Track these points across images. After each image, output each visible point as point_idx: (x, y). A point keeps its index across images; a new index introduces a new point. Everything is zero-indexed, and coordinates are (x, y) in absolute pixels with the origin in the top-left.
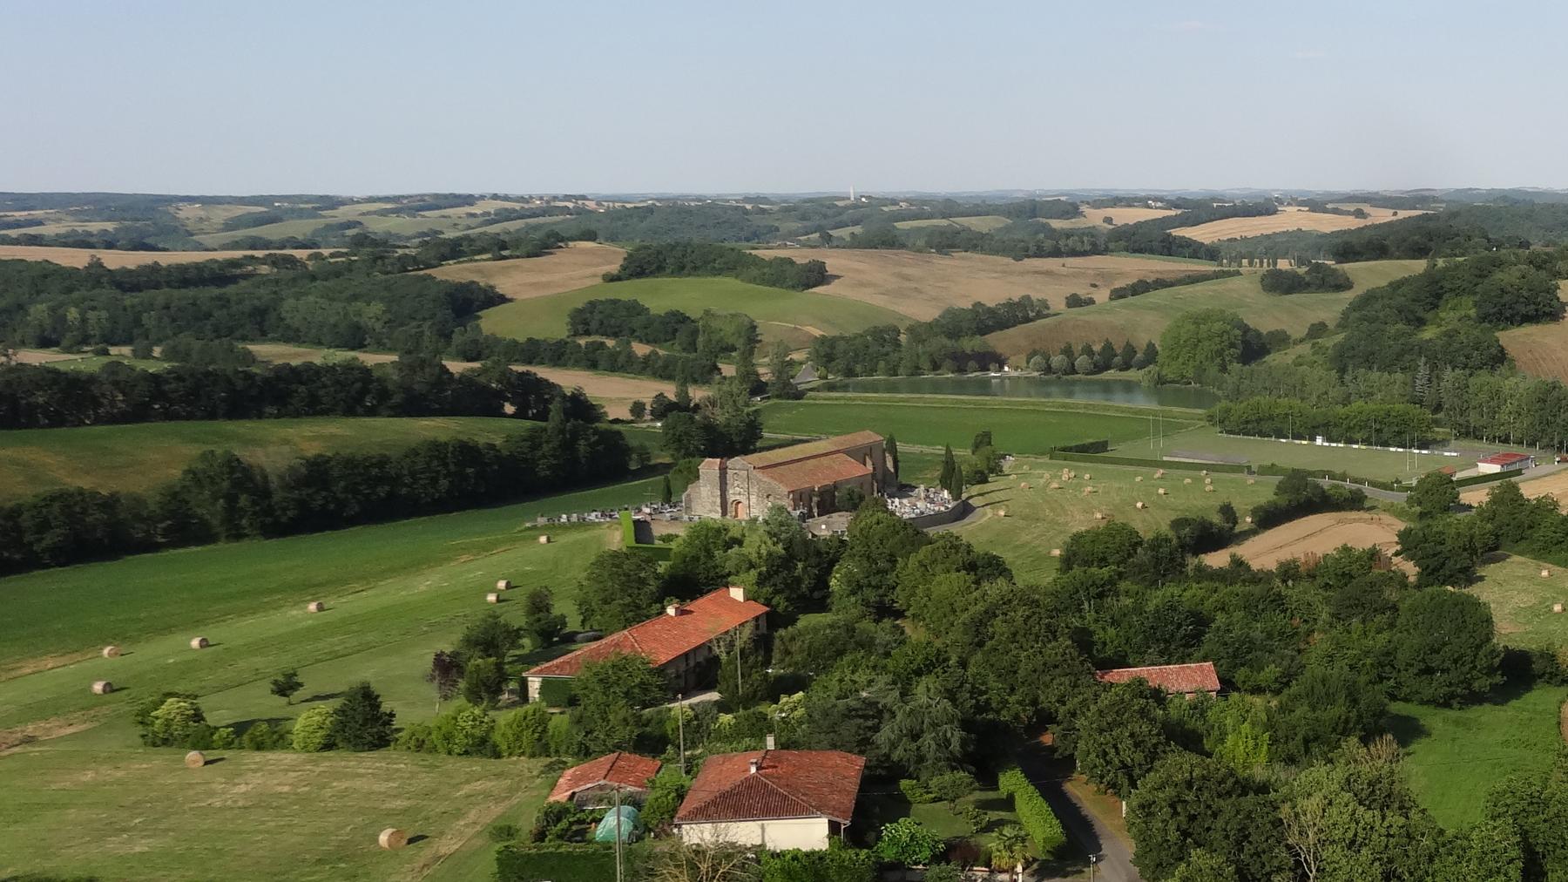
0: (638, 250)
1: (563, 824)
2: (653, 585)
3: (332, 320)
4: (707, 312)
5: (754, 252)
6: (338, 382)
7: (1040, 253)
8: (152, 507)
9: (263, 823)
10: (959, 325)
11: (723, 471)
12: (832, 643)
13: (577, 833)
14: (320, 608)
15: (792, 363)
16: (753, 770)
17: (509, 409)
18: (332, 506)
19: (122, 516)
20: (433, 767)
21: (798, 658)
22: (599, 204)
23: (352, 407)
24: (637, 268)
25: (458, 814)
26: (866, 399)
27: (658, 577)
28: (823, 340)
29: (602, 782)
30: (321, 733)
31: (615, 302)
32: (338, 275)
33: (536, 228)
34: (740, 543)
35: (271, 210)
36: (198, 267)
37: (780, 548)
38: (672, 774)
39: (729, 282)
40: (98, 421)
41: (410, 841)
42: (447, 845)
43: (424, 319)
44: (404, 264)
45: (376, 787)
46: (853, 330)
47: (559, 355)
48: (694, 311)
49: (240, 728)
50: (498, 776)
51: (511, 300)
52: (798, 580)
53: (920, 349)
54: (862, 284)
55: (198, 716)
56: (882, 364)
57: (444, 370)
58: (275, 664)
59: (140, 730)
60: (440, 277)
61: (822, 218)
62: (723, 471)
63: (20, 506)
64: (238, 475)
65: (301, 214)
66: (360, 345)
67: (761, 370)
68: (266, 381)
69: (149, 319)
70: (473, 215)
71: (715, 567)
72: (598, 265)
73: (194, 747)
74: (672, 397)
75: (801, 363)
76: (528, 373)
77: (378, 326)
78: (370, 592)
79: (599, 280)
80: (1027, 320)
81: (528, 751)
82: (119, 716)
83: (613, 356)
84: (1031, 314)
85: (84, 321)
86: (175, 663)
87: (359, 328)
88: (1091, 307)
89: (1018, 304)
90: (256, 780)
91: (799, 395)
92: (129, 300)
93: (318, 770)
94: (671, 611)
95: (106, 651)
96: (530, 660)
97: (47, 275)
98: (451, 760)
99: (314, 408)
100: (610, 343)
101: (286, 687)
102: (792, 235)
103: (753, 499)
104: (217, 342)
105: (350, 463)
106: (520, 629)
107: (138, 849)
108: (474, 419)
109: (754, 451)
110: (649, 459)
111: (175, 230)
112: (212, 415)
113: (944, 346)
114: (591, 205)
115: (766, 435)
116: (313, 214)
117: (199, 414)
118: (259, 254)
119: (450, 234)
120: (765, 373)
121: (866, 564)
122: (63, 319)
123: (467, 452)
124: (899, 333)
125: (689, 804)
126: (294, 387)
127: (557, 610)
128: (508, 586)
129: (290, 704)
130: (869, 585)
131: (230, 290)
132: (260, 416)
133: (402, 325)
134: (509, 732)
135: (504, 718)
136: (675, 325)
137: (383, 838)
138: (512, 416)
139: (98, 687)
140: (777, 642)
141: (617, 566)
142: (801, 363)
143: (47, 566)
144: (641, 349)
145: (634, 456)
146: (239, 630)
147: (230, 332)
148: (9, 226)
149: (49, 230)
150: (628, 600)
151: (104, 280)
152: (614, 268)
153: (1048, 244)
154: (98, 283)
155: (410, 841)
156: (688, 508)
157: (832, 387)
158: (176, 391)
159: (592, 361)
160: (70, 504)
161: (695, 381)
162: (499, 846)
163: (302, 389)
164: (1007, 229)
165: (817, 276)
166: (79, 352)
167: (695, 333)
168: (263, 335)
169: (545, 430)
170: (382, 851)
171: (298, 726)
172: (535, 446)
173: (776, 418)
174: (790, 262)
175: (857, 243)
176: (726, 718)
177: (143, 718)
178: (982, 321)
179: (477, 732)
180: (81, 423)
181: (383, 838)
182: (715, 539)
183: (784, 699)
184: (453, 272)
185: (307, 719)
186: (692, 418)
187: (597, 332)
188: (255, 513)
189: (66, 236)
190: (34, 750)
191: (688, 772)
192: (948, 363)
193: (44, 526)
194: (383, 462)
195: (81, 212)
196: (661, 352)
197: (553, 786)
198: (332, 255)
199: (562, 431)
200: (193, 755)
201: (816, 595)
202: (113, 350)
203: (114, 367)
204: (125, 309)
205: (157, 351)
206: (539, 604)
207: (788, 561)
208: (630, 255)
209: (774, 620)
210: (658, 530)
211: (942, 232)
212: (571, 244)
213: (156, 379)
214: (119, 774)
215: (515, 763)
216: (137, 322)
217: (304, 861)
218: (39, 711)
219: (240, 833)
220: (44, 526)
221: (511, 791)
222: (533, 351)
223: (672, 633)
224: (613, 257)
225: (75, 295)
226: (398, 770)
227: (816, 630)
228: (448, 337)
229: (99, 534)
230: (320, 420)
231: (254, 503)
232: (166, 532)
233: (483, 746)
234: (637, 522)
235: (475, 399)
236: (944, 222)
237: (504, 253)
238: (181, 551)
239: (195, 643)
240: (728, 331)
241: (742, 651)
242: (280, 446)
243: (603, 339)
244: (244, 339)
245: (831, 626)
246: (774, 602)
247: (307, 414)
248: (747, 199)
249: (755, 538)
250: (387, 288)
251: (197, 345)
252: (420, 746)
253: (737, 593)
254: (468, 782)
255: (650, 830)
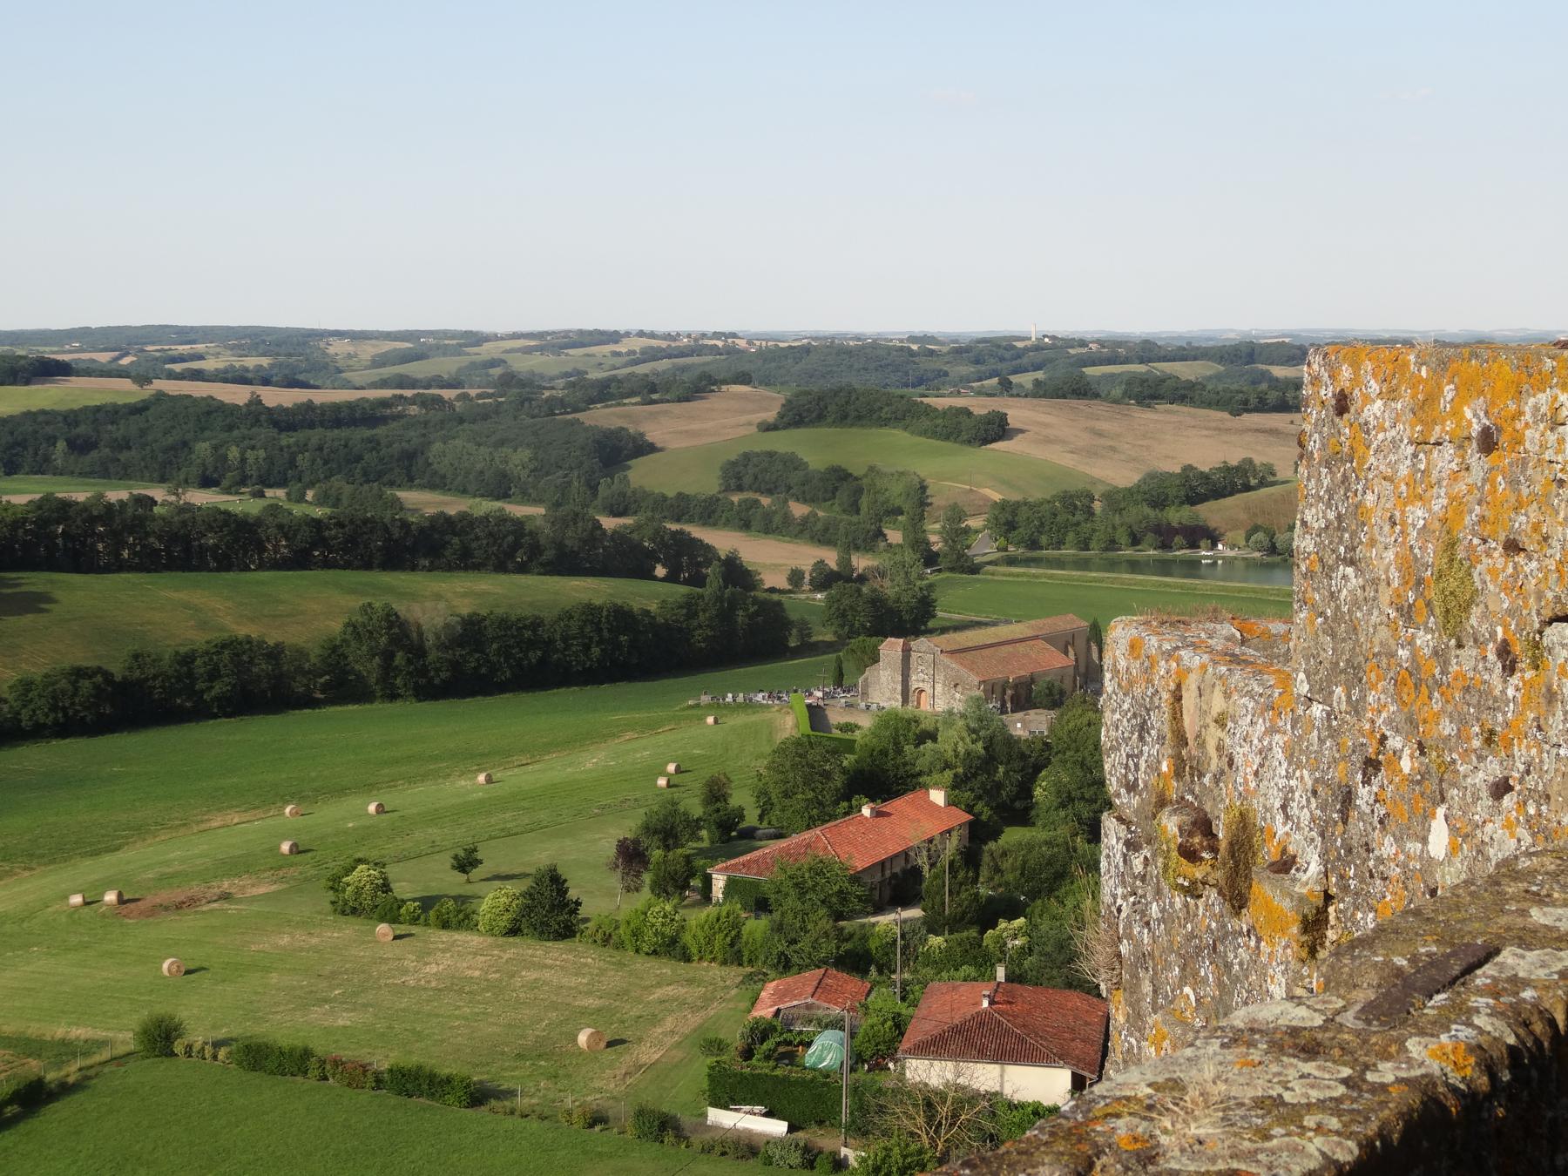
0: (797, 395)
1: (769, 1044)
2: (838, 781)
3: (479, 467)
4: (872, 469)
5: (926, 400)
6: (491, 534)
7: (1262, 406)
8: (313, 660)
9: (459, 1008)
10: (1157, 492)
11: (907, 652)
12: (1049, 863)
13: (783, 1056)
14: (489, 780)
15: (967, 531)
16: (985, 1004)
17: (660, 571)
18: (483, 670)
19: (285, 668)
20: (621, 964)
21: (1010, 877)
22: (750, 342)
23: (502, 564)
24: (796, 416)
25: (654, 1020)
26: (1051, 577)
27: (844, 771)
28: (1003, 506)
29: (810, 1000)
30: (507, 916)
31: (771, 455)
32: (486, 417)
33: (684, 369)
34: (934, 738)
35: (418, 346)
36: (351, 406)
37: (979, 746)
38: (884, 999)
39: (898, 436)
40: (261, 567)
41: (610, 1044)
42: (648, 1053)
43: (571, 469)
44: (553, 406)
45: (565, 981)
46: (1036, 495)
47: (709, 513)
48: (857, 467)
49: (427, 903)
50: (690, 982)
51: (661, 450)
52: (999, 786)
53: (1117, 520)
54: (1048, 441)
55: (386, 887)
56: (1071, 536)
57: (597, 525)
58: (457, 837)
59: (331, 895)
60: (588, 423)
61: (997, 359)
62: (907, 652)
63: (194, 651)
64: (396, 630)
65: (445, 351)
66: (504, 495)
67: (933, 538)
68: (422, 530)
69: (303, 460)
70: (617, 354)
71: (905, 764)
72: (754, 412)
73: (382, 919)
74: (833, 564)
75: (977, 532)
76: (681, 532)
77: (524, 474)
78: (537, 766)
79: (754, 429)
80: (1247, 488)
81: (720, 957)
82: (306, 880)
83: (768, 517)
84: (1253, 482)
85: (243, 460)
86: (354, 829)
87: (505, 476)
88: (403, 421)
89: (1237, 468)
90: (446, 961)
91: (975, 569)
92: (286, 440)
93: (506, 956)
94: (866, 811)
95: (288, 810)
96: (712, 855)
97: (212, 411)
98: (641, 959)
99: (466, 562)
100: (765, 501)
101: (466, 863)
102: (965, 380)
103: (939, 688)
104: (366, 487)
105: (504, 623)
106: (699, 819)
107: (341, 1022)
108: (623, 581)
109: (930, 632)
110: (809, 635)
111: (325, 367)
112: (368, 566)
113: (1146, 517)
114: (742, 344)
115: (940, 614)
116: (457, 351)
117: (510, 566)
118: (408, 393)
119: (595, 375)
120: (936, 542)
121: (1079, 773)
122: (225, 458)
123: (622, 617)
124: (1092, 500)
125: (912, 1036)
126: (447, 538)
127: (734, 802)
128: (678, 770)
129: (468, 881)
130: (1083, 798)
131: (380, 431)
132: (414, 568)
133: (548, 474)
134: (700, 935)
135: (697, 917)
136: (837, 483)
137: (582, 1038)
138: (663, 580)
139: (285, 847)
140: (986, 858)
141: (801, 756)
142: (977, 532)
143: (215, 716)
144: (799, 510)
145: (794, 631)
146: (414, 797)
147: (379, 476)
148: (174, 360)
149: (209, 365)
150: (811, 795)
151: (263, 417)
152: (771, 416)
153: (1273, 396)
154: (257, 422)
155: (610, 1044)
156: (865, 694)
157: (1012, 561)
158: (335, 538)
159: (743, 522)
160: (238, 651)
161: (857, 548)
162: (711, 1060)
163: (456, 540)
164: (1218, 377)
165: (997, 429)
166: (237, 493)
167: (859, 491)
168: (410, 481)
169: (701, 597)
170: (581, 1052)
171: (484, 907)
172: (692, 615)
173: (952, 600)
174: (966, 412)
175: (1041, 391)
176: (936, 941)
177: (335, 884)
178: (1192, 489)
179: (668, 931)
180: (247, 569)
181: (582, 1038)
182: (909, 732)
183: (1003, 924)
184: (602, 417)
185: (494, 901)
186: (859, 591)
187: (750, 488)
188: (409, 673)
189: (226, 371)
190: (232, 908)
191: (903, 999)
192: (1150, 537)
193: (214, 675)
194: (536, 624)
195: (240, 347)
196: (821, 514)
197: (755, 1000)
198: (479, 396)
199: (720, 599)
200: (383, 928)
201: (1018, 804)
202: (269, 493)
203: (274, 509)
204: (281, 449)
205: (310, 495)
206: (716, 793)
207: (989, 760)
208: (789, 401)
209: (979, 833)
210: (836, 716)
211: (1143, 380)
212: (724, 388)
213: (317, 524)
214: (314, 941)
215: (704, 969)
216: (292, 463)
217: (503, 1053)
218: (241, 865)
219: (437, 1016)
220: (214, 675)
221: (707, 1000)
222: (682, 507)
223: (867, 837)
224: (770, 404)
225: (236, 433)
226: (586, 965)
227: (1030, 847)
228: (594, 489)
229: (264, 685)
230: (472, 575)
231: (409, 661)
232: (325, 688)
233: (672, 947)
234: (809, 706)
235: (628, 560)
236: (1142, 368)
237: (655, 396)
238: (339, 708)
239: (372, 808)
240: (895, 492)
241: (951, 864)
242: (437, 600)
243: (757, 496)
244: (392, 484)
245: (1048, 843)
246: (977, 808)
247: (458, 568)
248: (913, 339)
249: (952, 732)
250: (535, 433)
251: (348, 489)
252: (606, 940)
253: (938, 797)
254: (659, 985)
255: (864, 1061)
